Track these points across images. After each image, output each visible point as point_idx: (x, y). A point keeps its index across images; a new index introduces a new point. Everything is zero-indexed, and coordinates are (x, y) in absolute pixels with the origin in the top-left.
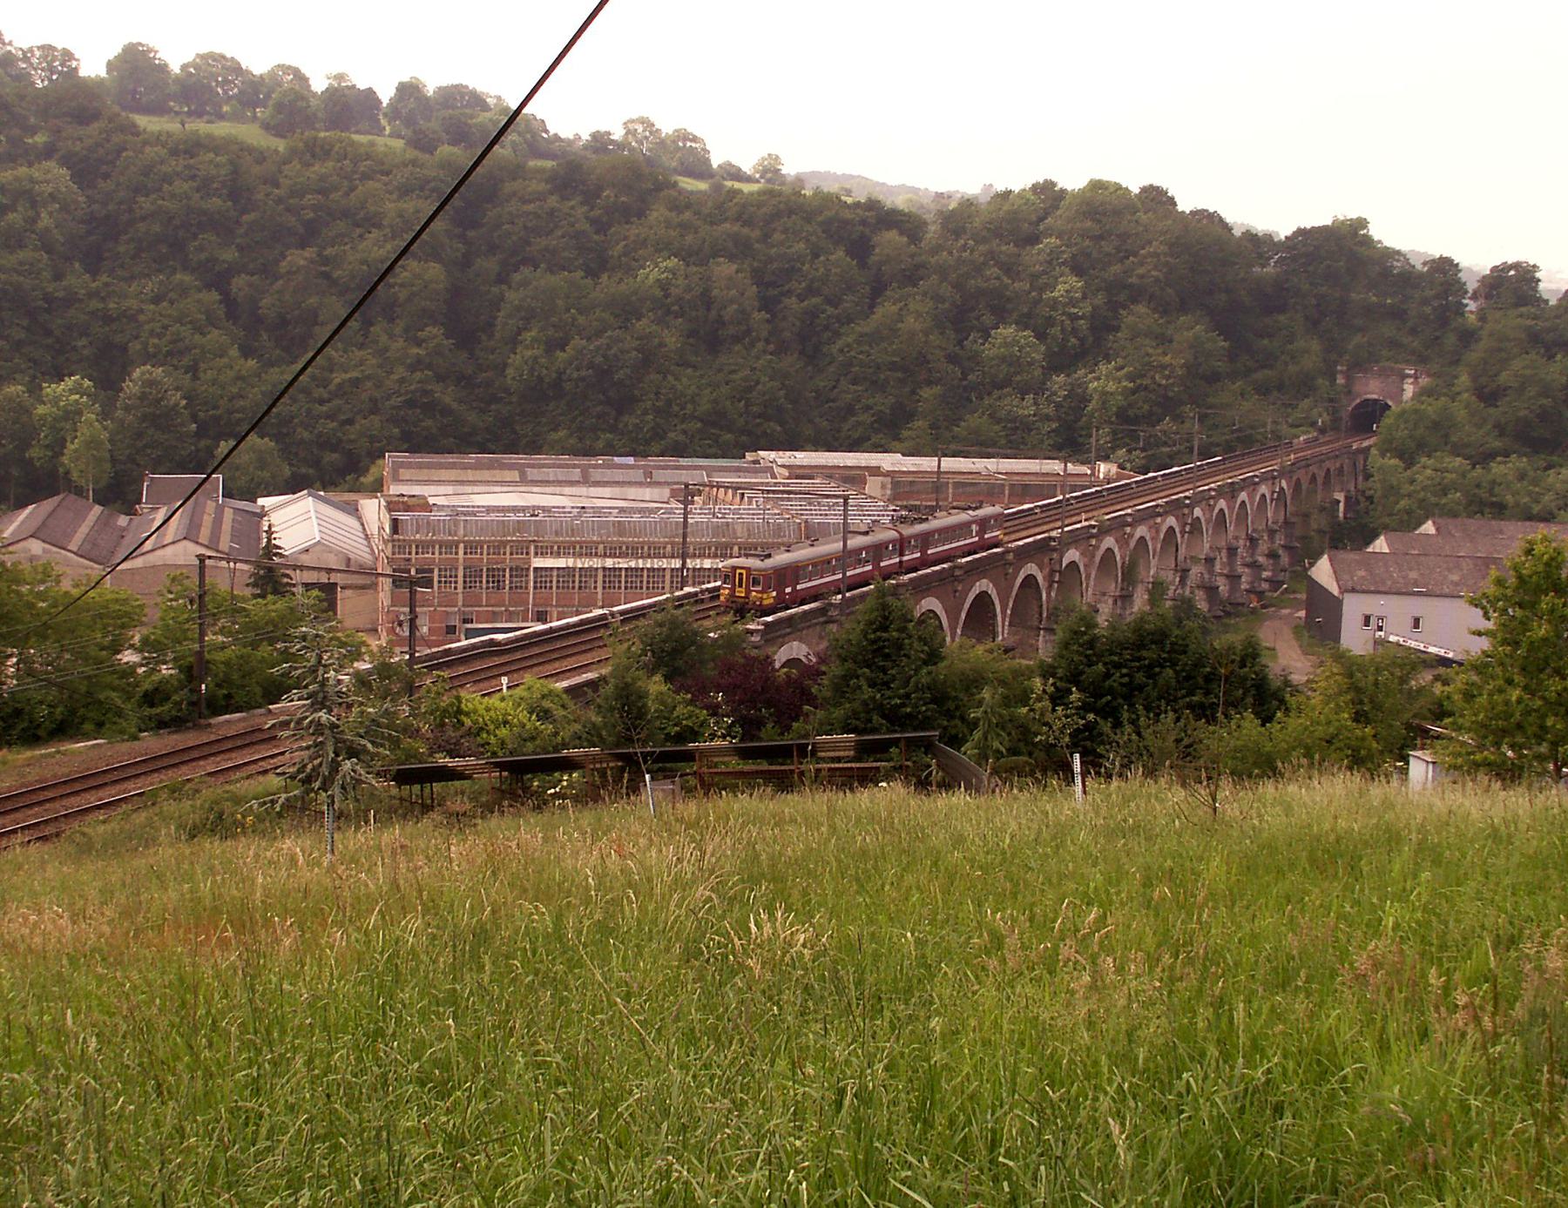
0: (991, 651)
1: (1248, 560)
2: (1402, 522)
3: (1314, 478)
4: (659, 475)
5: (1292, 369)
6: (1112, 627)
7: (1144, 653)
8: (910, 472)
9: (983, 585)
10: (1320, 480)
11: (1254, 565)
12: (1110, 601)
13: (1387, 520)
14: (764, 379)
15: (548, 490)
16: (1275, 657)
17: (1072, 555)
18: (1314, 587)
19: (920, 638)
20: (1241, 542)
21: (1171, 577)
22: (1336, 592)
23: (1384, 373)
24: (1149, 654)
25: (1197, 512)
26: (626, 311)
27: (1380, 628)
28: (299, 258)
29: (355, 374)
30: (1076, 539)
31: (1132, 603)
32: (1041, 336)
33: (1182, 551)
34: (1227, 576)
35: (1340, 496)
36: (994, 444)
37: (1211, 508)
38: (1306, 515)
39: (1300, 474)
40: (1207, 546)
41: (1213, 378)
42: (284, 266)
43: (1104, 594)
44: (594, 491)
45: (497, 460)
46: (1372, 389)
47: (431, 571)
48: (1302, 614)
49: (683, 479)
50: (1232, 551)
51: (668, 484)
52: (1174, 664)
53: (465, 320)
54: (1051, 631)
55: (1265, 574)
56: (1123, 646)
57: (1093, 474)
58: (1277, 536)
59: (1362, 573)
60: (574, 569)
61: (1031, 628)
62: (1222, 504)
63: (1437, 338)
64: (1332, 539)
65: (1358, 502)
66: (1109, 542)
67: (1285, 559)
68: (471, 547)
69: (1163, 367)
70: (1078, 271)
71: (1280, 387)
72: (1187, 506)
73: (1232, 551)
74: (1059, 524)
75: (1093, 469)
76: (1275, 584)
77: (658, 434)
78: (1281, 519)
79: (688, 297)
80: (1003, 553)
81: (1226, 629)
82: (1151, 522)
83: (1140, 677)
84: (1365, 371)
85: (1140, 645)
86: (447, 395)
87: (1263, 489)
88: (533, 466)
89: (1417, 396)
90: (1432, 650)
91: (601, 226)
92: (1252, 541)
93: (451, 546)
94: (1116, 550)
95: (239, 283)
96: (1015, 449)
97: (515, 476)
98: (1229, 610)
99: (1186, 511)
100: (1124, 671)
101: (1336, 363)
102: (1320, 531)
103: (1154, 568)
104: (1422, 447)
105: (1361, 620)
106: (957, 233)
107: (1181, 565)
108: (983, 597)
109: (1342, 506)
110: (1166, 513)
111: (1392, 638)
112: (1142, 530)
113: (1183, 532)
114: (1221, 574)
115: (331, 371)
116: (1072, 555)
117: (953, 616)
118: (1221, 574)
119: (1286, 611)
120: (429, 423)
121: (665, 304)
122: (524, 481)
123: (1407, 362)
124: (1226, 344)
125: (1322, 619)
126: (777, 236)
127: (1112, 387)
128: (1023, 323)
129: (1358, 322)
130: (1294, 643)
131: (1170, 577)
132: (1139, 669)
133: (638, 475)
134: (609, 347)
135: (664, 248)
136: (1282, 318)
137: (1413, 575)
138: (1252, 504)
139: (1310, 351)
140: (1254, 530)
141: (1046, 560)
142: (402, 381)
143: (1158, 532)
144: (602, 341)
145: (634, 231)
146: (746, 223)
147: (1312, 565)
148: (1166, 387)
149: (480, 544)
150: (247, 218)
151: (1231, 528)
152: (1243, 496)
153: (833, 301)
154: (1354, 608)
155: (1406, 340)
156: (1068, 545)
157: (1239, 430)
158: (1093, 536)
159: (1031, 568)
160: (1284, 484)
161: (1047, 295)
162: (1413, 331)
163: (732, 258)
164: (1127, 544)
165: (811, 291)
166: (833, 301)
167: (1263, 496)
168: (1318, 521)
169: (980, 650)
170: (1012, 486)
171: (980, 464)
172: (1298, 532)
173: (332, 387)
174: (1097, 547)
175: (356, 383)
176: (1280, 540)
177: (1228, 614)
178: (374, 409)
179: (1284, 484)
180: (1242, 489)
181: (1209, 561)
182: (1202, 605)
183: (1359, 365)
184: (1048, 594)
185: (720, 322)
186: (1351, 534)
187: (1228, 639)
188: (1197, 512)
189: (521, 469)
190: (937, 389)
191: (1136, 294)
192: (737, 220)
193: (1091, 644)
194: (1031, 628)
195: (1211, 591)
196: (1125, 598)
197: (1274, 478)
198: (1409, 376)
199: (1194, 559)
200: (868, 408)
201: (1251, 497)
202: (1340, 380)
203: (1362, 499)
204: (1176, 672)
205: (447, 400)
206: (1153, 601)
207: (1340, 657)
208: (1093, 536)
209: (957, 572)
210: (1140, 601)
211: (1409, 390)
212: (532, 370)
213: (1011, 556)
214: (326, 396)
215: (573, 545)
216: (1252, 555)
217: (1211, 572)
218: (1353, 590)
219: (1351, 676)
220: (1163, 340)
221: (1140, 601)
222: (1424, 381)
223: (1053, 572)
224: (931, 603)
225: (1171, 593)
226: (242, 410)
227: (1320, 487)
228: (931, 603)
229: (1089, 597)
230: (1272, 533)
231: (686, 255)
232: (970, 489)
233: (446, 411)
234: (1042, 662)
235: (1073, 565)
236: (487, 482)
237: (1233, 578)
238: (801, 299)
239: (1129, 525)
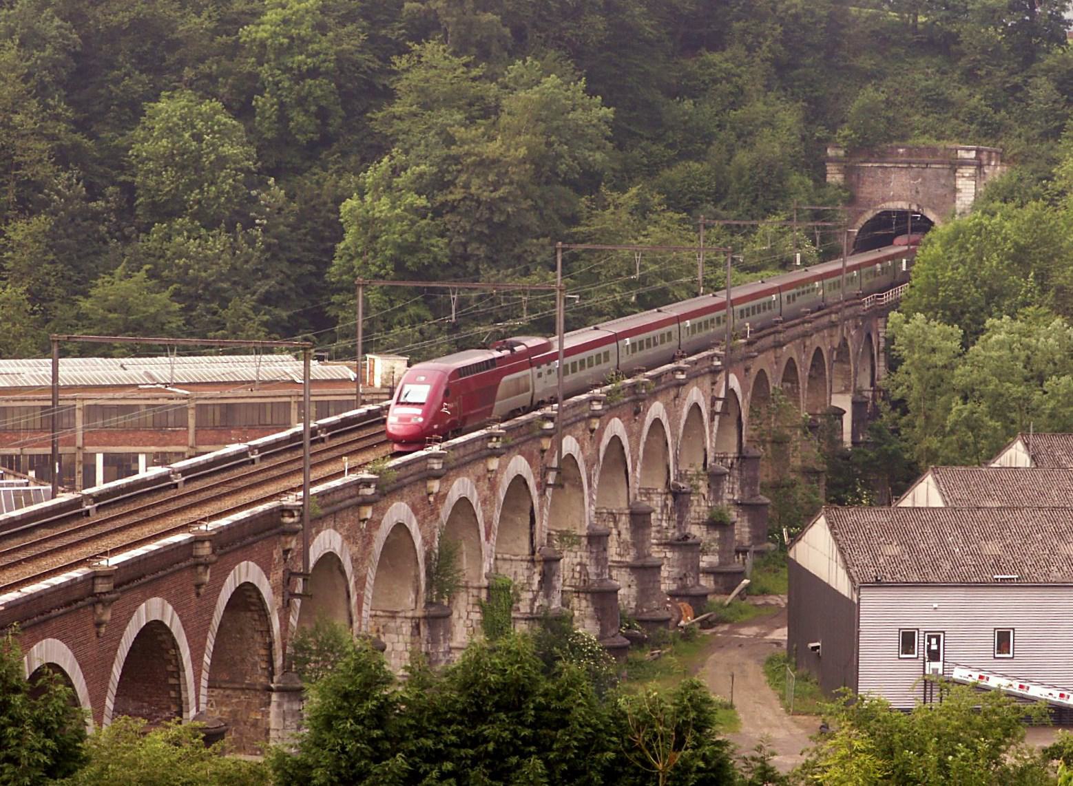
0: (177, 742)
1: (673, 533)
2: (963, 446)
3: (791, 366)
5: (743, 158)
6: (418, 678)
7: (488, 731)
8: (30, 388)
9: (154, 609)
10: (803, 373)
11: (683, 544)
12: (407, 628)
13: (934, 442)
16: (734, 722)
17: (327, 540)
18: (803, 581)
19: (39, 725)
20: (657, 501)
21: (522, 579)
22: (842, 585)
23: (918, 159)
24: (495, 730)
25: (569, 445)
27: (934, 656)
30: (334, 508)
31: (449, 631)
32: (242, 110)
33: (543, 524)
34: (633, 568)
35: (843, 402)
36: (161, 329)
37: (596, 435)
38: (780, 442)
39: (763, 362)
40: (590, 510)
41: (588, 181)
43: (393, 615)
46: (895, 190)
48: (781, 634)
50: (639, 519)
52: (543, 750)
54: (294, 693)
55: (706, 561)
56: (440, 717)
57: (360, 380)
58: (726, 485)
59: (893, 550)
61: (251, 688)
62: (616, 426)
63: (1016, 88)
64: (831, 486)
65: (876, 413)
66: (398, 511)
67: (743, 531)
69: (485, 164)
71: (718, 196)
72: (548, 434)
73: (639, 519)
74: (298, 480)
75: (359, 370)
76: (726, 579)
78: (733, 452)
81: (640, 672)
82: (479, 469)
84: (882, 157)
85: (478, 715)
87: (695, 394)
88: (962, 149)
89: (984, 201)
90: (1035, 691)
92: (679, 497)
94: (414, 527)
96: (200, 335)
98: (637, 636)
99: (546, 444)
100: (448, 766)
101: (823, 143)
102: (808, 472)
103: (492, 558)
104: (995, 297)
105: (895, 642)
107: (543, 551)
108: (154, 633)
109: (847, 420)
110: (508, 449)
111: (958, 674)
112: (461, 487)
113: (543, 486)
114: (621, 565)
116: (327, 540)
117: (96, 671)
118: (621, 565)
119: (748, 632)
123: (962, 136)
124: (608, 112)
125: (821, 644)
127: (383, 207)
128: (205, 87)
129: (866, 62)
130: (768, 691)
131: (520, 573)
132: (475, 761)
136: (716, 57)
137: (992, 548)
138: (674, 426)
139: (779, 125)
140: (681, 476)
141: (277, 554)
143: (493, 487)
147: (795, 538)
148: (492, 206)
151: (637, 475)
152: (657, 409)
154: (880, 617)
155: (959, 93)
156: (318, 521)
157: (643, 281)
158: (366, 502)
159: (247, 572)
160: (734, 383)
161: (247, 33)
162: (970, 76)
164: (434, 512)
167: (696, 407)
168: (805, 452)
169: (157, 740)
170: (201, 408)
171: (136, 369)
172: (766, 474)
174: (374, 524)
176: (731, 491)
177: (638, 642)
179: (734, 383)
180: (654, 396)
181: (597, 540)
182: (587, 628)
183: (870, 146)
186: (869, 473)
187: (647, 693)
188: (569, 445)
190: (41, 222)
193: (380, 715)
194: (251, 688)
195: (603, 597)
196: (435, 620)
197: (715, 372)
198: (964, 163)
199: (566, 537)
201: (672, 411)
202: (834, 176)
203: (885, 407)
204: (548, 763)
206: (494, 625)
207: (865, 718)
208: (366, 502)
209: (101, 587)
210: (465, 629)
211: (967, 189)
213: (205, 550)
216: (681, 522)
217: (601, 561)
218: (878, 584)
219: (889, 752)
221: (465, 629)
222: (996, 172)
223: (289, 576)
224: (51, 650)
225: (524, 607)
227: (803, 384)
228: (51, 650)
229: (365, 622)
230: (715, 479)
232: (119, 420)
234: (281, 757)
235: (330, 560)
237: (645, 571)
239: (437, 477)
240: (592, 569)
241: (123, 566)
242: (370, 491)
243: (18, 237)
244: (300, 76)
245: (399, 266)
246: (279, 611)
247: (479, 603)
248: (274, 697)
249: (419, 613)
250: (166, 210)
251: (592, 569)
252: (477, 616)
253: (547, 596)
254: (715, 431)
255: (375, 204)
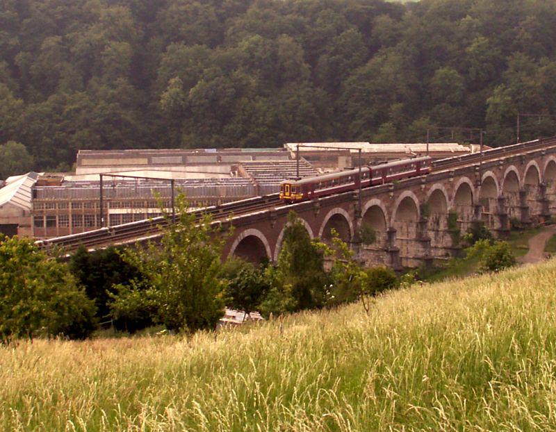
4: (225, 159)
12: (415, 225)
14: (303, 101)
15: (164, 168)
26: (228, 66)
28: (52, 41)
29: (77, 106)
42: (44, 46)
43: (411, 222)
44: (189, 168)
45: (137, 153)
47: (55, 217)
49: (359, 147)
51: (229, 163)
53: (142, 73)
60: (131, 214)
68: (75, 204)
69: (530, 88)
70: (487, 34)
77: (244, 133)
79: (263, 57)
80: (312, 204)
82: (446, 181)
83: (105, 276)
86: (128, 116)
88: (155, 156)
91: (222, 19)
93: (65, 204)
95: (20, 58)
97: (145, 161)
106: (420, 15)
115: (65, 104)
120: (116, 132)
121: (251, 63)
122: (150, 164)
126: (319, 21)
133: (214, 159)
134: (217, 86)
135: (252, 29)
142: (103, 108)
144: (214, 82)
145: (238, 21)
146: (304, 14)
149: (80, 203)
150: (26, 21)
153: (348, 57)
163: (291, 33)
165: (336, 52)
166: (348, 57)
173: (65, 113)
175: (78, 111)
178: (87, 126)
184: (355, 224)
185: (283, 69)
189: (149, 158)
191: (519, 48)
192: (297, 12)
200: (362, 116)
205: (128, 118)
212: (176, 100)
213: (318, 205)
214: (61, 118)
215: (130, 201)
220: (531, 73)
226: (14, 127)
231: (265, 33)
233: (127, 124)
236: (130, 165)
238: (332, 54)
240: (499, 209)
241: (279, 210)
242: (392, 188)
243: (393, 109)
244: (483, 62)
245: (503, 116)
246: (353, 221)
247: (447, 219)
248: (351, 244)
249: (418, 221)
250: (440, 100)
251: (499, 209)
252: (446, 222)
253: (477, 216)
254: (502, 184)
255: (497, 98)
